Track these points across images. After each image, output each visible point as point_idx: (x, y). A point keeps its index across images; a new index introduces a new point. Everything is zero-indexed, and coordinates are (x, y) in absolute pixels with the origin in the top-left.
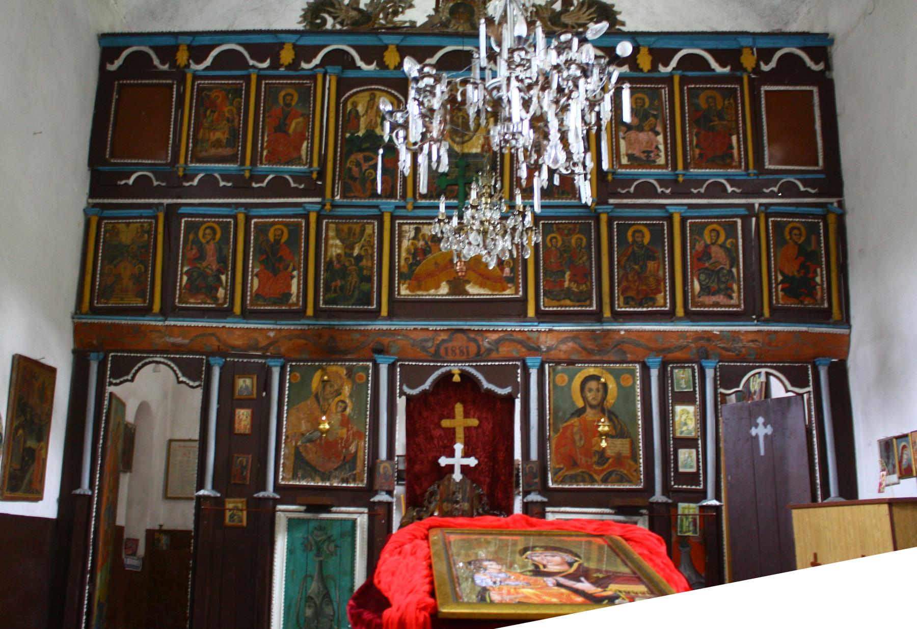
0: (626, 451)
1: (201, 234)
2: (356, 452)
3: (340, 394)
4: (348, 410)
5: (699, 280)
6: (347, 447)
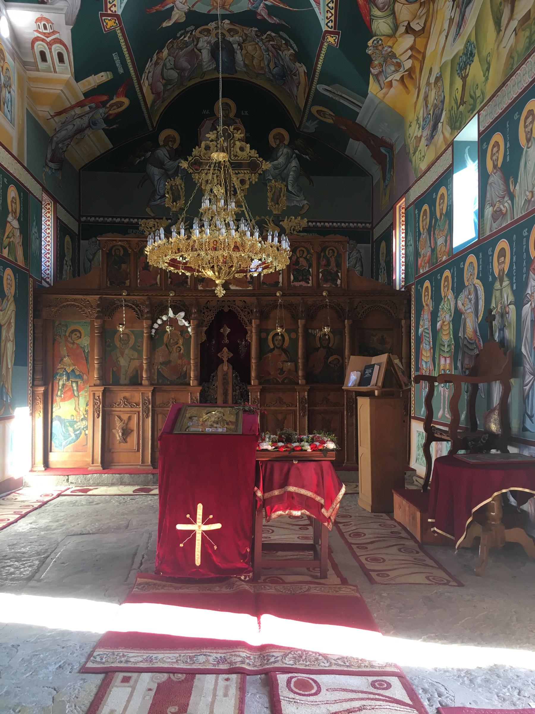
1: (327, 253)
2: (186, 370)
3: (178, 344)
4: (182, 351)
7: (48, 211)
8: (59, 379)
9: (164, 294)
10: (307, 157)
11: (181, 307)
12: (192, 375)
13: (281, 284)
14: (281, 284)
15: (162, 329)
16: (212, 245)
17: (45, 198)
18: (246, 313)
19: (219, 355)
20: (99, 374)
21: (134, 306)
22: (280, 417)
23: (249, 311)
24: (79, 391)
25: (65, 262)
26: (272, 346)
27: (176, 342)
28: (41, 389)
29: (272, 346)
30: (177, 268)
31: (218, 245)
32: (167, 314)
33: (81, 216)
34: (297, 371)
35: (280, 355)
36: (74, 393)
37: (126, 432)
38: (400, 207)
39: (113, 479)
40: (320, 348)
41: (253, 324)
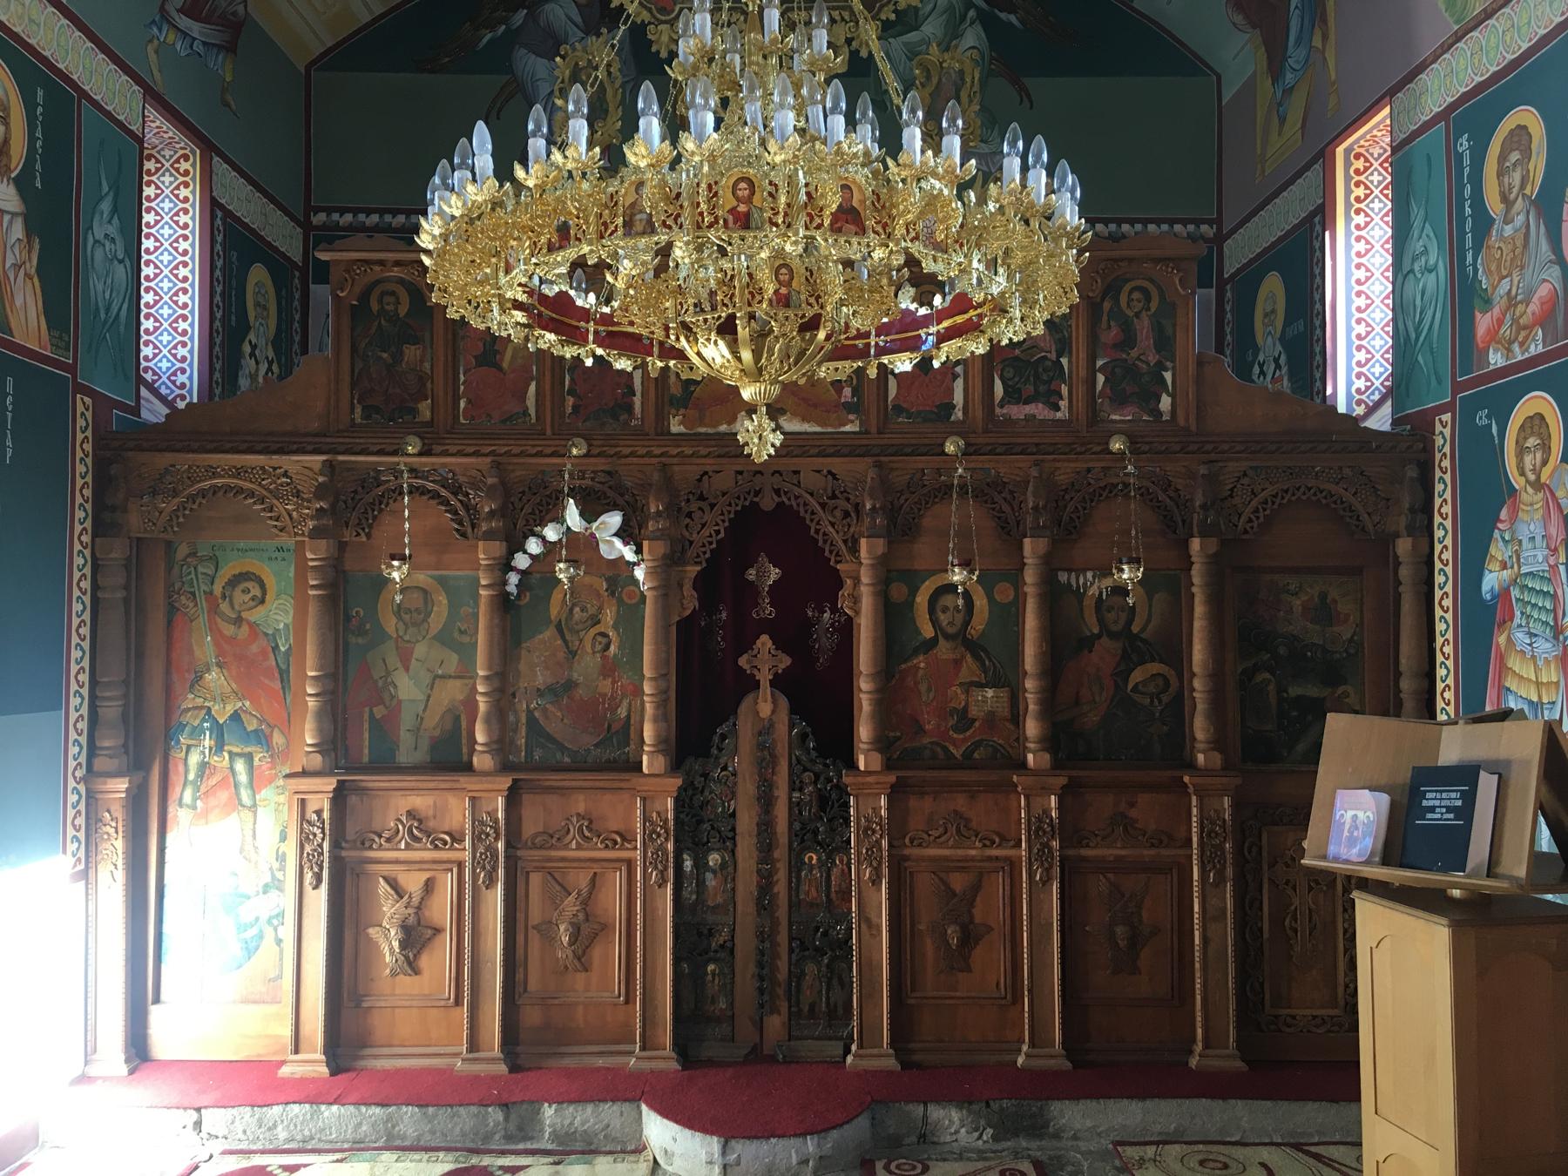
0: (1003, 710)
2: (628, 717)
4: (612, 648)
5: (1001, 378)
6: (614, 710)
7: (181, 179)
8: (189, 747)
9: (549, 451)
10: (1013, 18)
11: (610, 493)
12: (648, 733)
13: (958, 414)
14: (958, 414)
15: (539, 577)
16: (726, 201)
17: (158, 128)
18: (838, 513)
19: (743, 661)
20: (320, 731)
21: (444, 492)
22: (958, 882)
23: (850, 508)
24: (253, 786)
25: (247, 349)
26: (928, 631)
27: (592, 617)
28: (119, 787)
29: (928, 631)
30: (573, 335)
31: (756, 200)
32: (560, 520)
33: (310, 209)
34: (1017, 718)
35: (957, 663)
36: (238, 794)
37: (416, 937)
38: (1348, 151)
39: (360, 1124)
40: (1099, 636)
41: (863, 553)
